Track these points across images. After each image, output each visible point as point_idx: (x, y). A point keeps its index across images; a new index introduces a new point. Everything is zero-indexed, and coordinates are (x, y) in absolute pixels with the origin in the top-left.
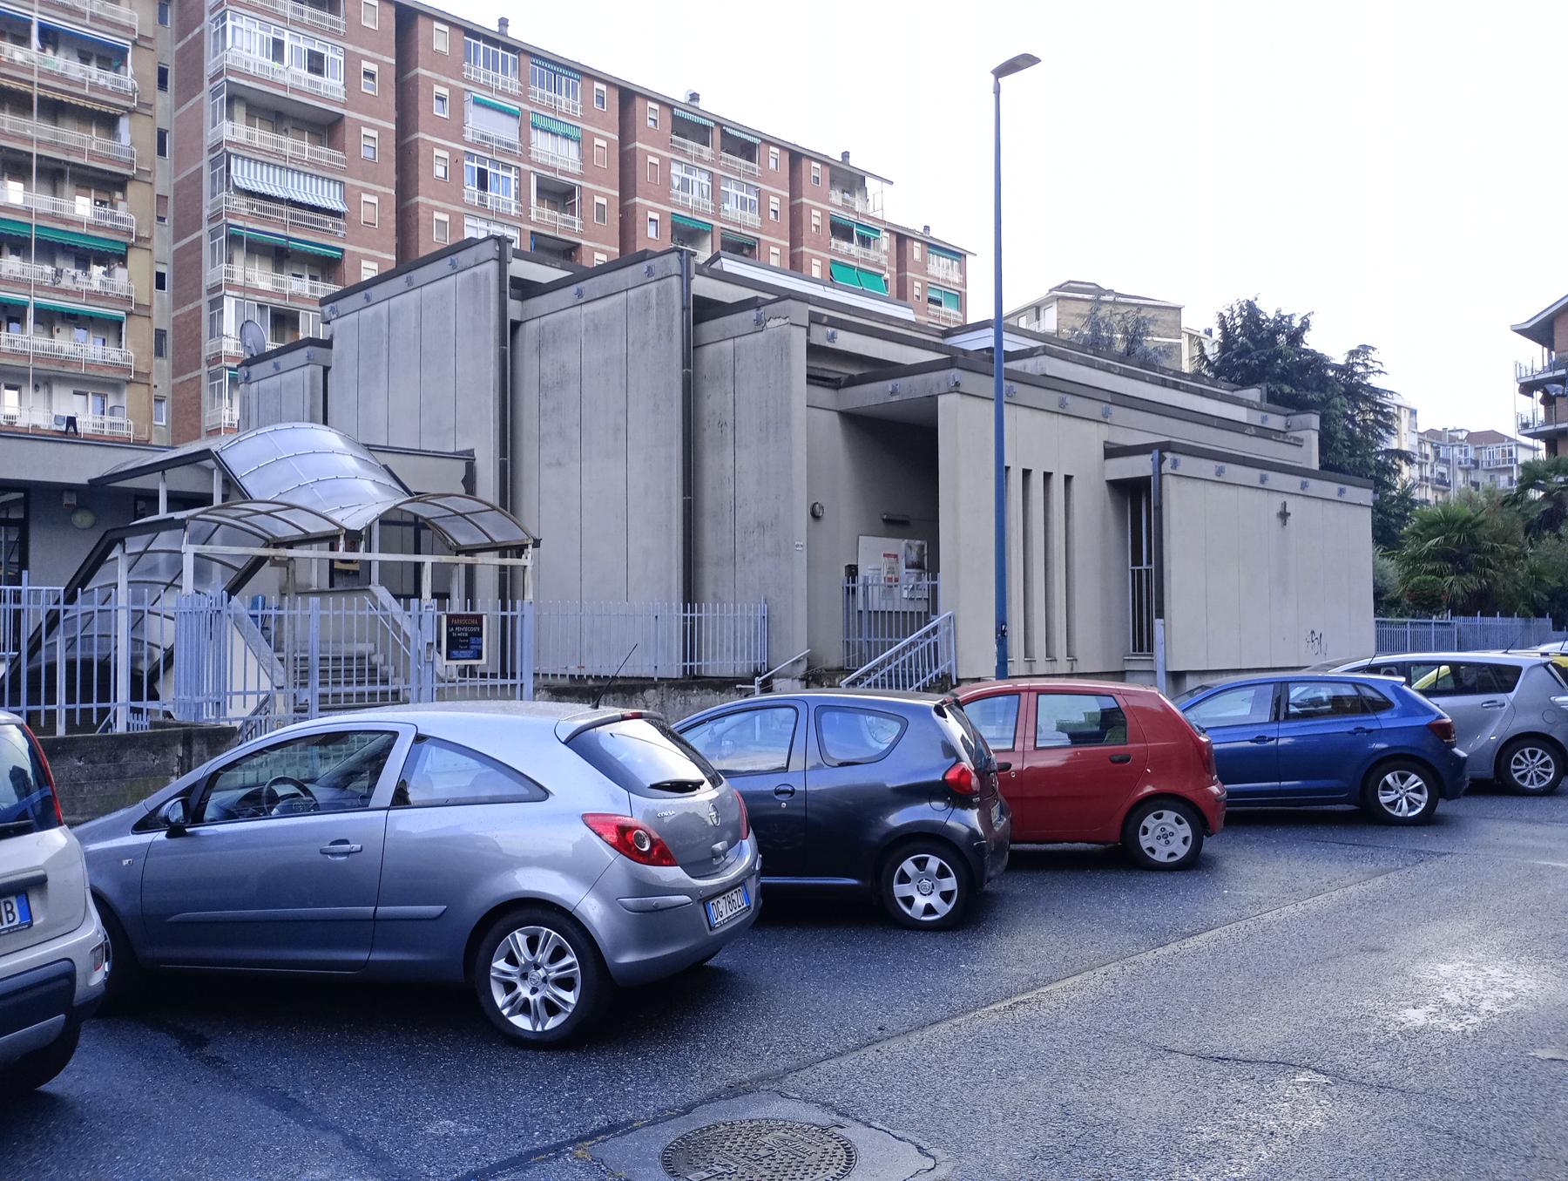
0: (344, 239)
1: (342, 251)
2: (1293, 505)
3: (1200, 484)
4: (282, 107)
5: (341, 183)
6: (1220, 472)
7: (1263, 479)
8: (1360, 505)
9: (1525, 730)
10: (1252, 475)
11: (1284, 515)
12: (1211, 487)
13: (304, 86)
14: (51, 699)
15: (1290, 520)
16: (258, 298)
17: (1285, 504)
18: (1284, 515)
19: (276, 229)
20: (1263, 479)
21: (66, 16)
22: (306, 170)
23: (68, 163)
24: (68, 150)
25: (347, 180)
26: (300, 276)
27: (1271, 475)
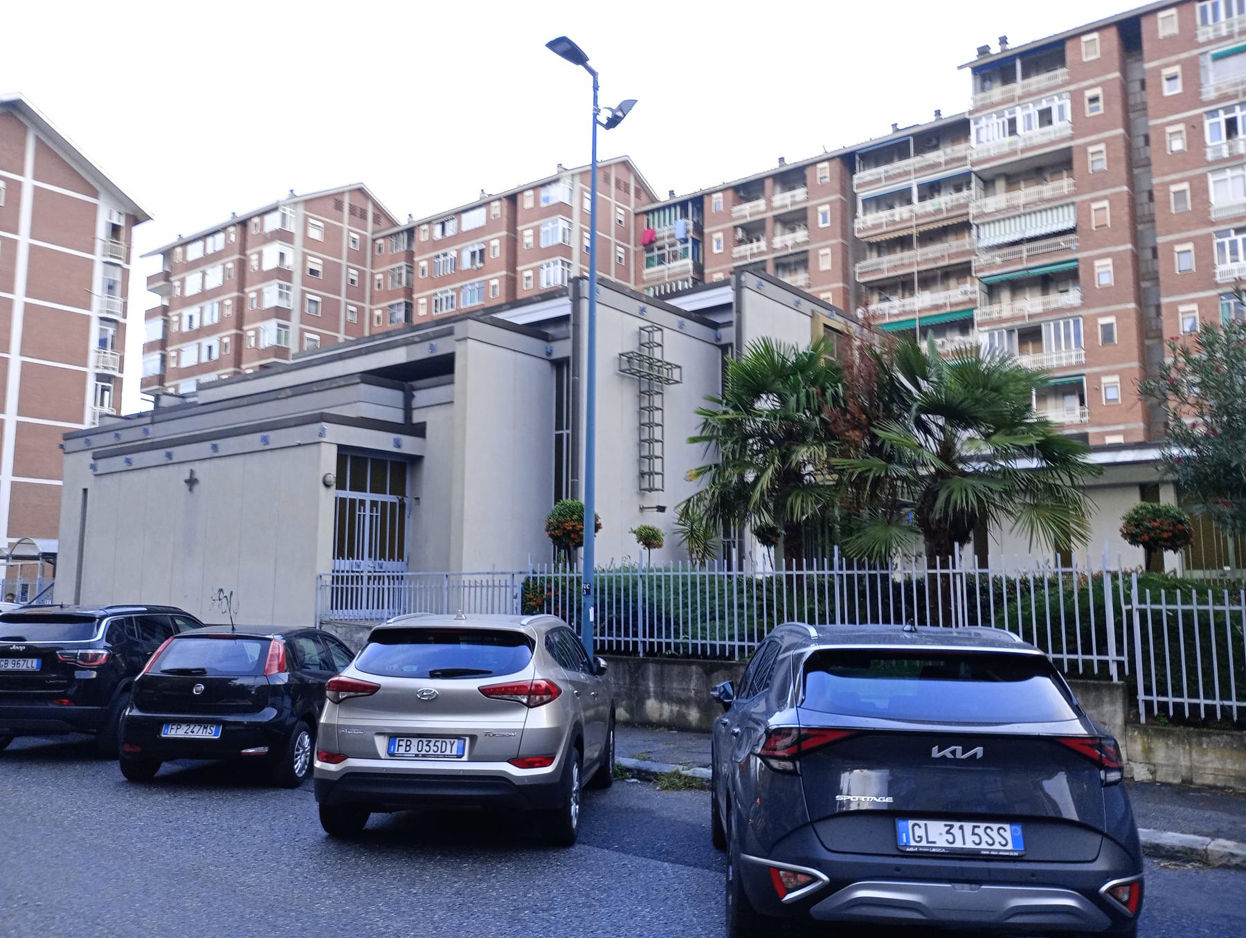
0: (1078, 251)
1: (1076, 260)
2: (201, 470)
3: (116, 476)
4: (1037, 163)
5: (1073, 204)
6: (265, 440)
7: (169, 456)
8: (300, 445)
9: (365, 862)
10: (254, 440)
11: (192, 482)
12: (125, 476)
13: (1045, 139)
14: (1103, 649)
15: (196, 488)
16: (1004, 325)
17: (192, 472)
18: (192, 482)
19: (1025, 263)
20: (169, 456)
21: (931, 171)
22: (1039, 208)
23: (937, 268)
24: (935, 260)
25: (1076, 199)
26: (1067, 291)
27: (272, 435)
